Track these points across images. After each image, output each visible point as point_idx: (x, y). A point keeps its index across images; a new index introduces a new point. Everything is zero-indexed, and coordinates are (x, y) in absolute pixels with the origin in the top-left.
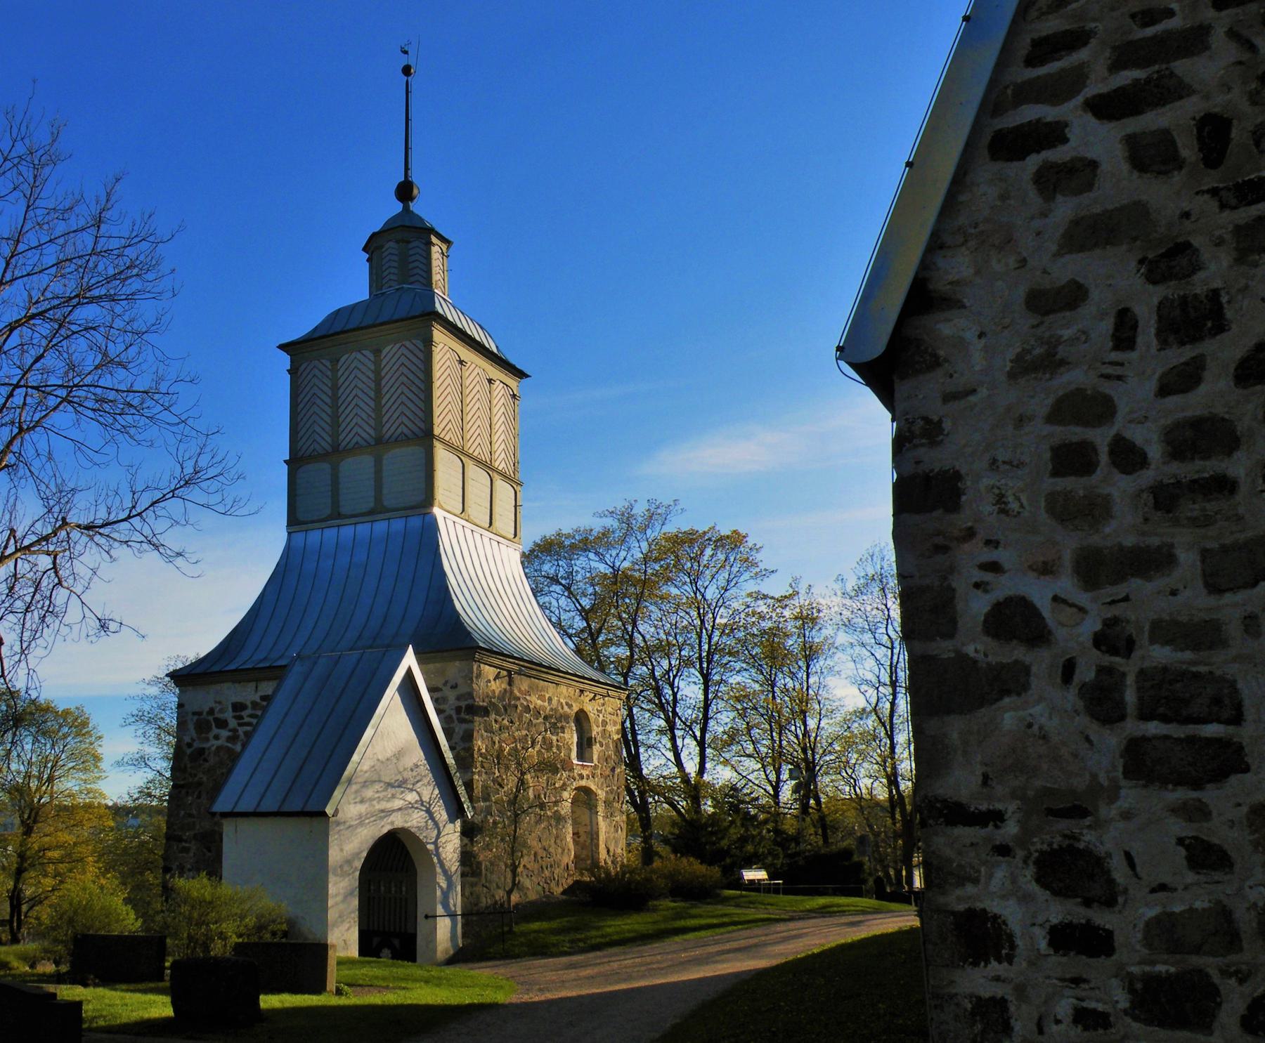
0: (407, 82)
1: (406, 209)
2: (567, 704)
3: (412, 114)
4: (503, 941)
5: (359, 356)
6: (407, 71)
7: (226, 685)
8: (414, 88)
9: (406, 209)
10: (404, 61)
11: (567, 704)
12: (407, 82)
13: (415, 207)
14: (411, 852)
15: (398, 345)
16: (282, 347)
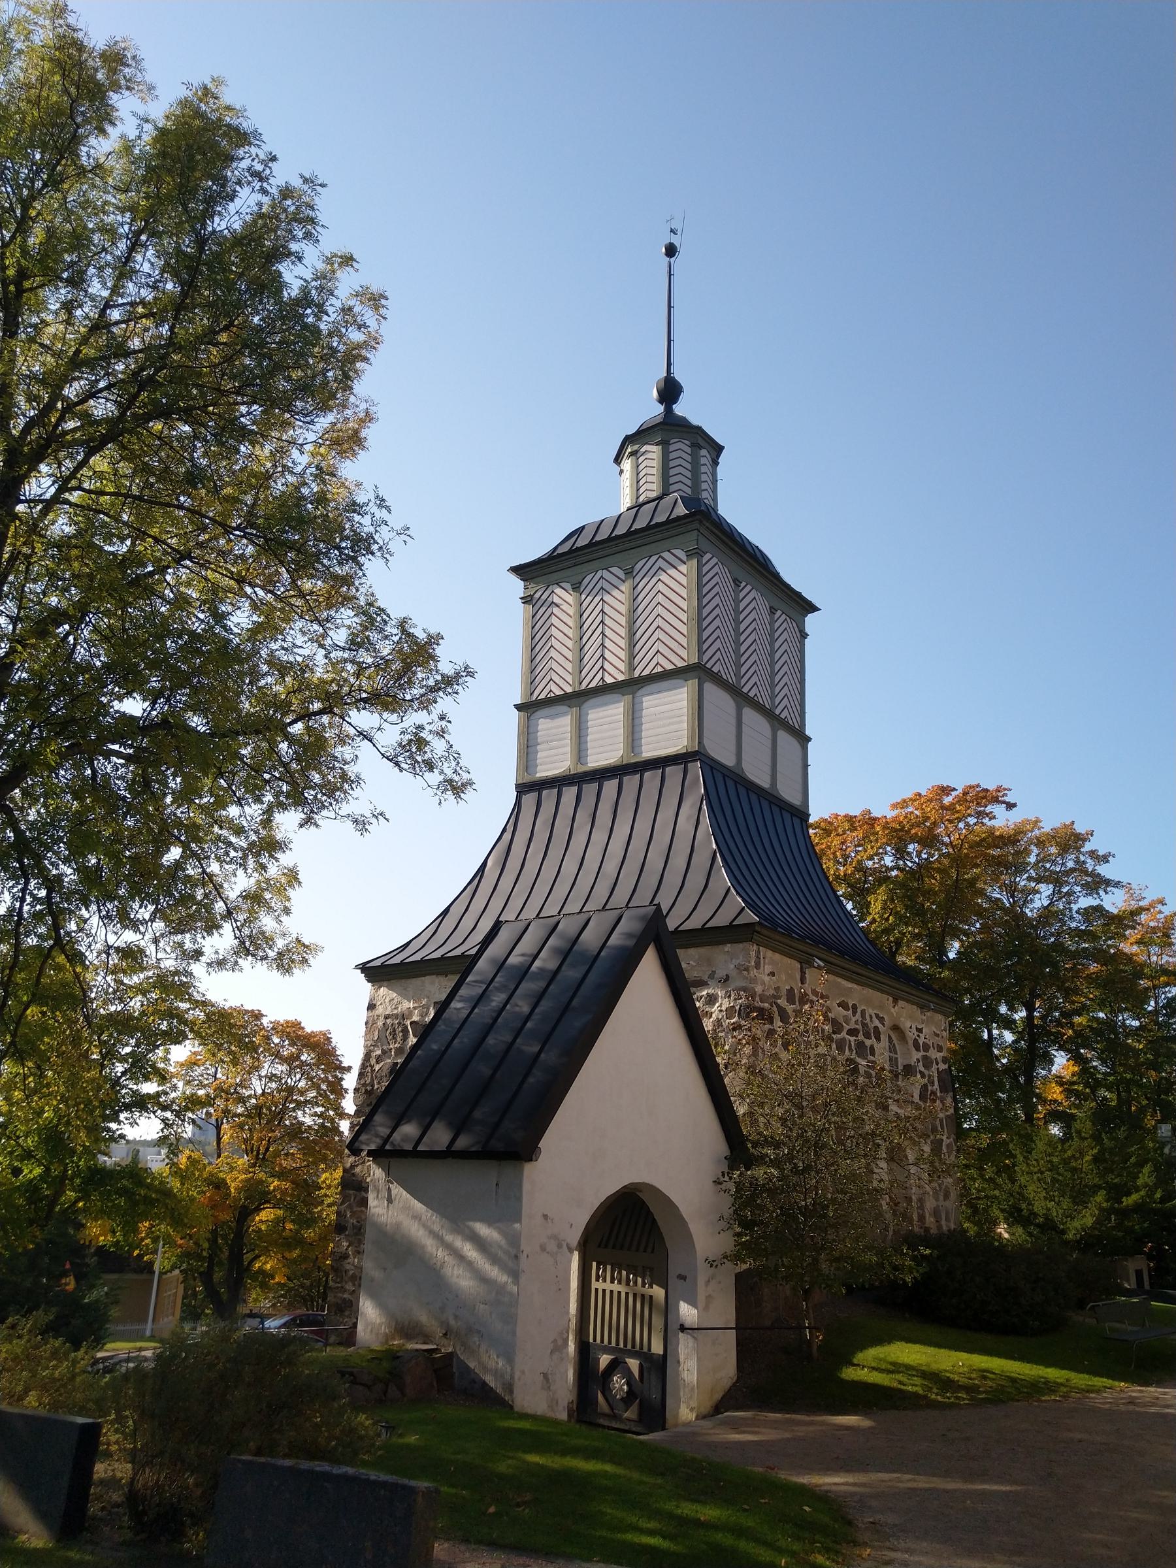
0: (670, 263)
1: (669, 411)
2: (877, 1016)
3: (676, 302)
4: (332, 294)
5: (606, 574)
6: (671, 251)
7: (427, 979)
8: (677, 271)
9: (669, 411)
10: (669, 238)
11: (877, 1016)
12: (670, 263)
13: (679, 409)
14: (660, 1223)
15: (654, 558)
16: (518, 570)
